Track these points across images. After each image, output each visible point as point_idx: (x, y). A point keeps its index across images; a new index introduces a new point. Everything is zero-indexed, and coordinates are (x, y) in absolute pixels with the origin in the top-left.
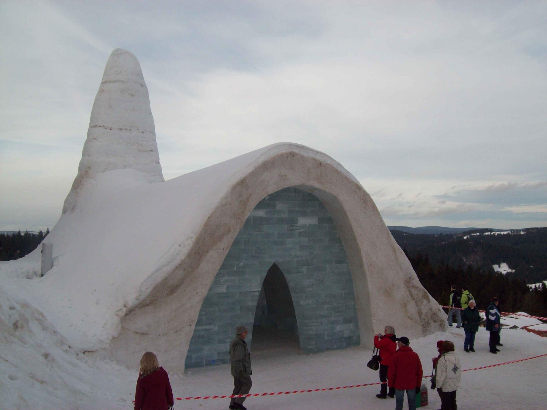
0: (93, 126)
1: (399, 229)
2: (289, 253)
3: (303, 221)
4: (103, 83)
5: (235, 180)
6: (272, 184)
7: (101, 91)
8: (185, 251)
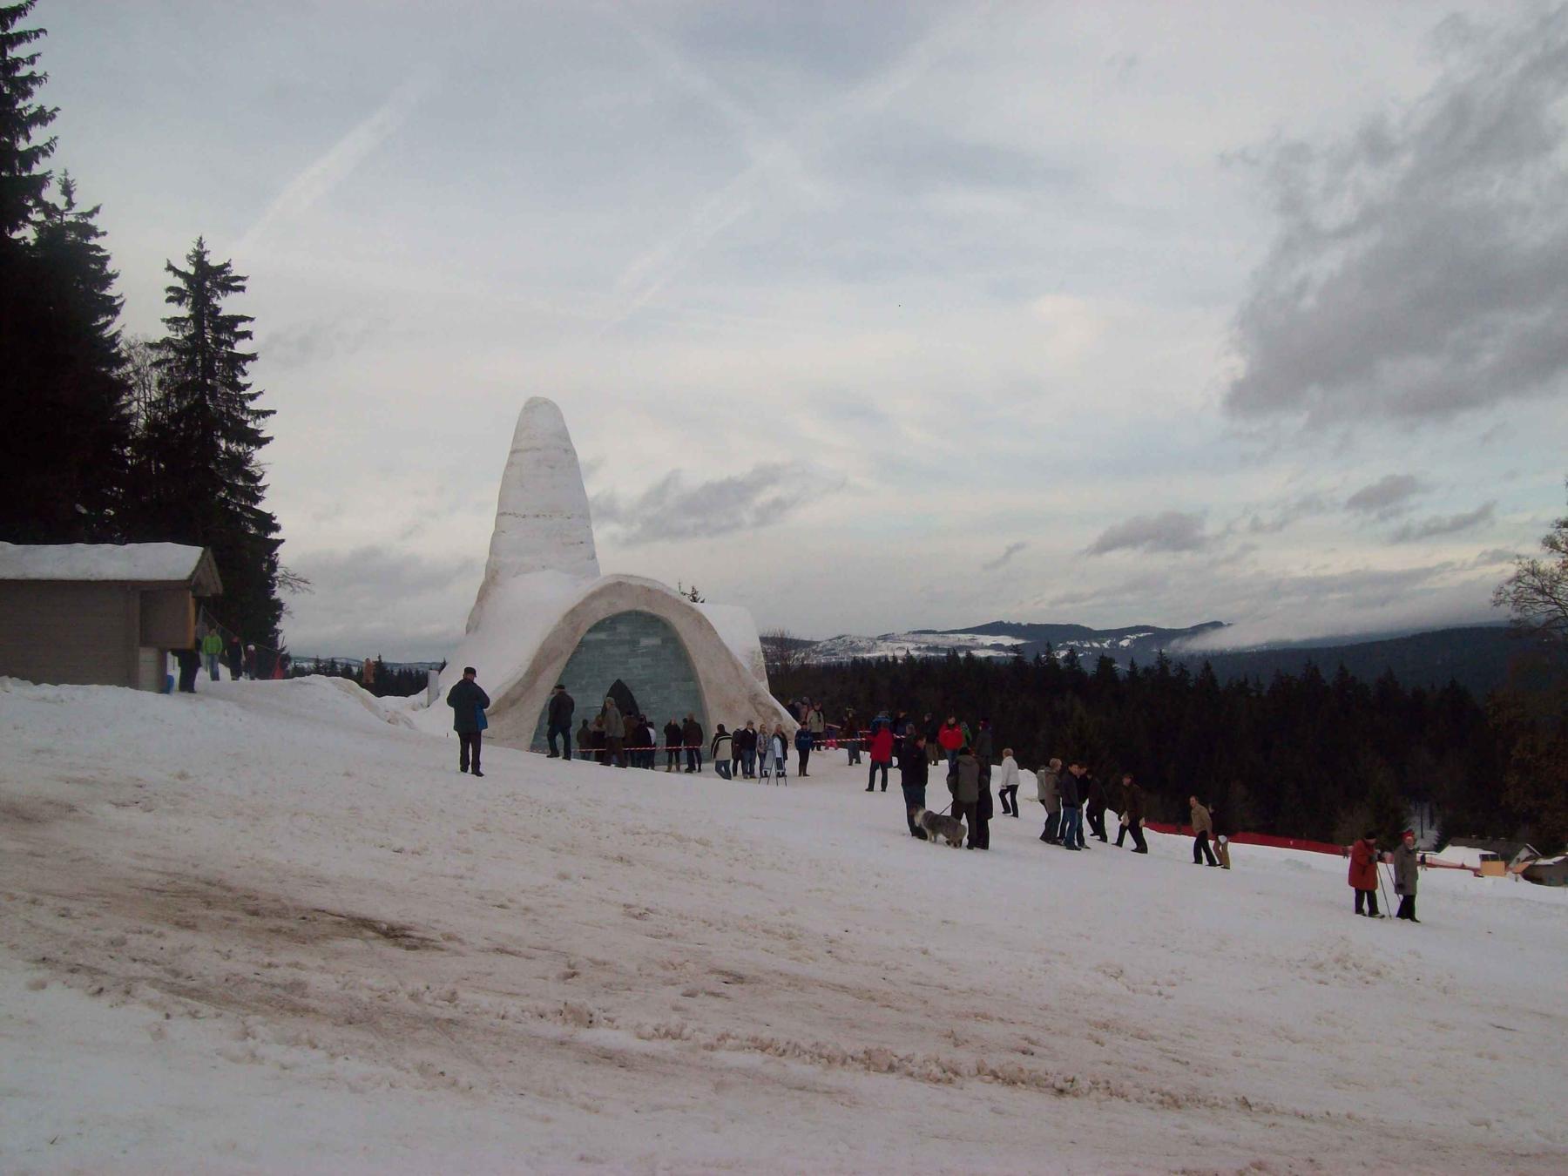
0: (500, 514)
1: (1315, 646)
2: (634, 671)
3: (645, 642)
4: (513, 452)
5: (567, 610)
6: (602, 610)
7: (510, 464)
8: (524, 670)
